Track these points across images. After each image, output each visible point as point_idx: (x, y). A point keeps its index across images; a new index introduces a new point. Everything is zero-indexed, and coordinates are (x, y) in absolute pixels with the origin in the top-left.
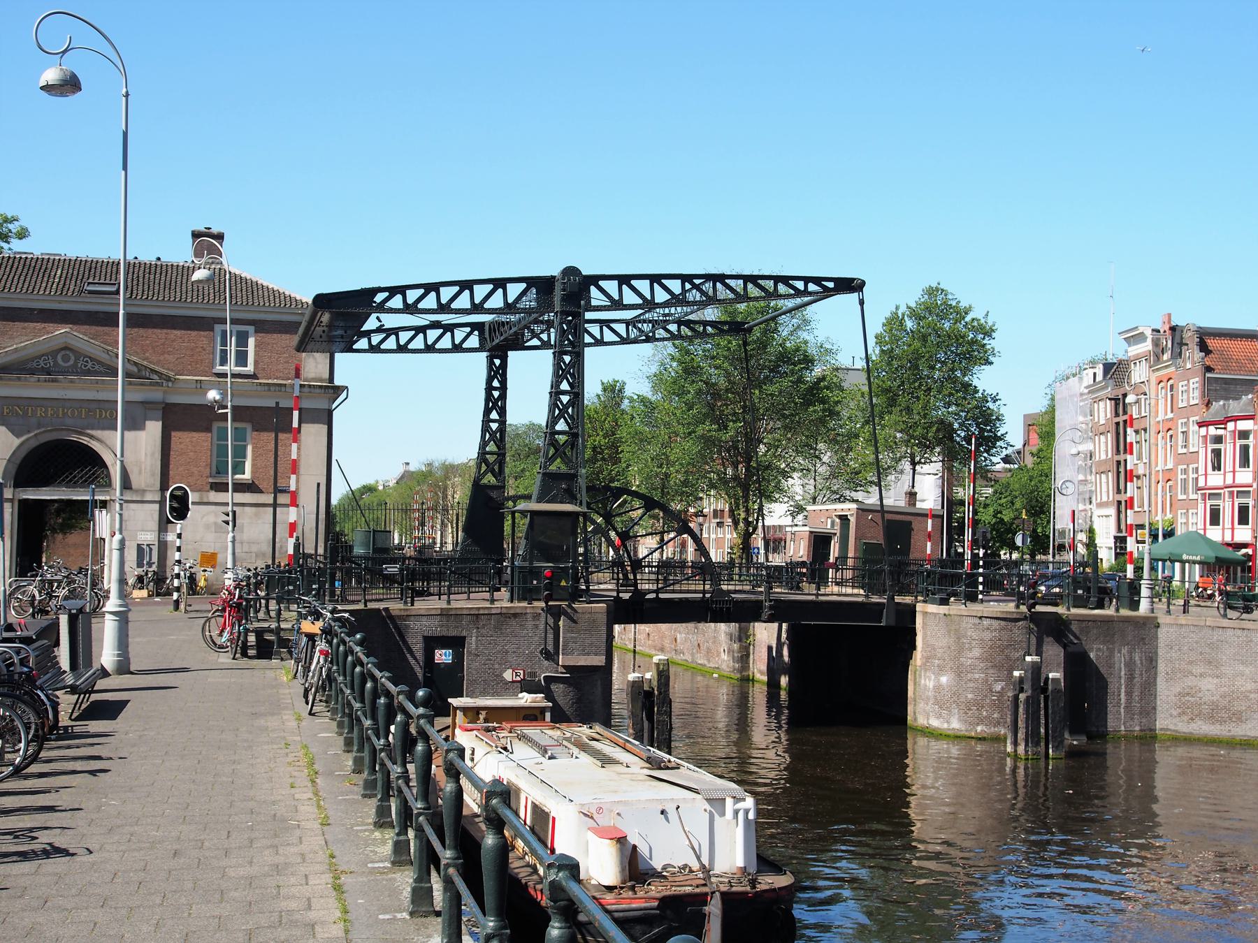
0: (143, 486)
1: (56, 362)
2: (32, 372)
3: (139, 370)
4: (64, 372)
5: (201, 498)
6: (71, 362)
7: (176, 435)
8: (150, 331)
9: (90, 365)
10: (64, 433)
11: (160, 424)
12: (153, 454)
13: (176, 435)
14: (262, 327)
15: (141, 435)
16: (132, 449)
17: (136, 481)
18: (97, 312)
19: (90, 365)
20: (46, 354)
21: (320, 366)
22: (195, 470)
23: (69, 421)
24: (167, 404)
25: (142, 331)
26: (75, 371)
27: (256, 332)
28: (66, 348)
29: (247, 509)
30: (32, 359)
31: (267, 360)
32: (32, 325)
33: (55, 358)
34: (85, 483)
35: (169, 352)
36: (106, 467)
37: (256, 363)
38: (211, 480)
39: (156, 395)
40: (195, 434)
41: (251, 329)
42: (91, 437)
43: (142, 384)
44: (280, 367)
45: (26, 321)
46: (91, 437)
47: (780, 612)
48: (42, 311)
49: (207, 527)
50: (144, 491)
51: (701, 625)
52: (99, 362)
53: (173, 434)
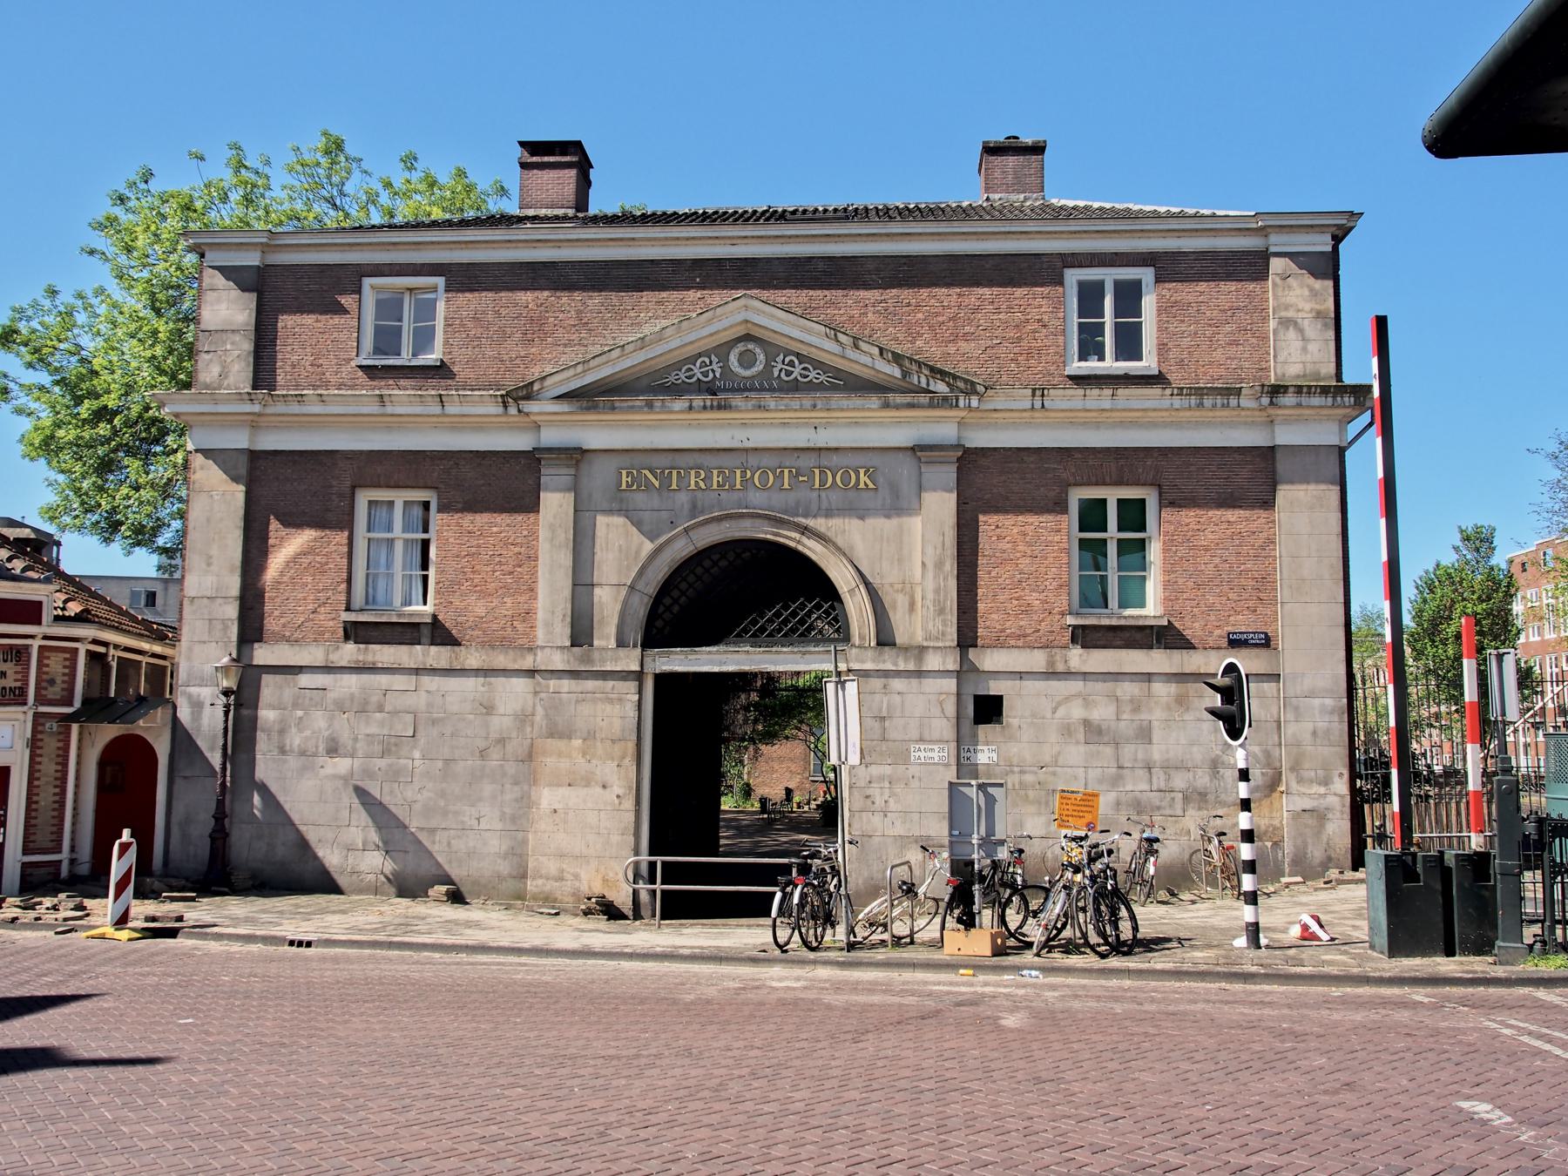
0: (919, 638)
1: (726, 368)
2: (676, 390)
3: (905, 374)
4: (744, 388)
5: (1051, 663)
6: (759, 367)
7: (991, 526)
8: (924, 292)
9: (797, 372)
10: (747, 523)
11: (951, 499)
12: (939, 565)
13: (991, 526)
14: (1169, 267)
15: (916, 524)
16: (891, 555)
17: (908, 628)
18: (810, 259)
19: (797, 372)
20: (707, 353)
21: (1312, 347)
22: (1034, 599)
23: (757, 498)
24: (967, 451)
25: (906, 294)
26: (766, 385)
27: (1159, 280)
28: (748, 338)
29: (1030, 685)
30: (677, 366)
31: (1186, 342)
32: (676, 295)
33: (724, 359)
34: (800, 633)
35: (966, 337)
36: (840, 600)
37: (1162, 348)
38: (1070, 620)
39: (941, 428)
40: (1033, 519)
41: (1146, 275)
42: (805, 530)
43: (911, 406)
44: (1218, 355)
45: (664, 289)
46: (805, 530)
47: (41, 562)
48: (698, 263)
49: (1067, 730)
50: (922, 649)
51: (238, 572)
52: (818, 364)
53: (982, 518)
